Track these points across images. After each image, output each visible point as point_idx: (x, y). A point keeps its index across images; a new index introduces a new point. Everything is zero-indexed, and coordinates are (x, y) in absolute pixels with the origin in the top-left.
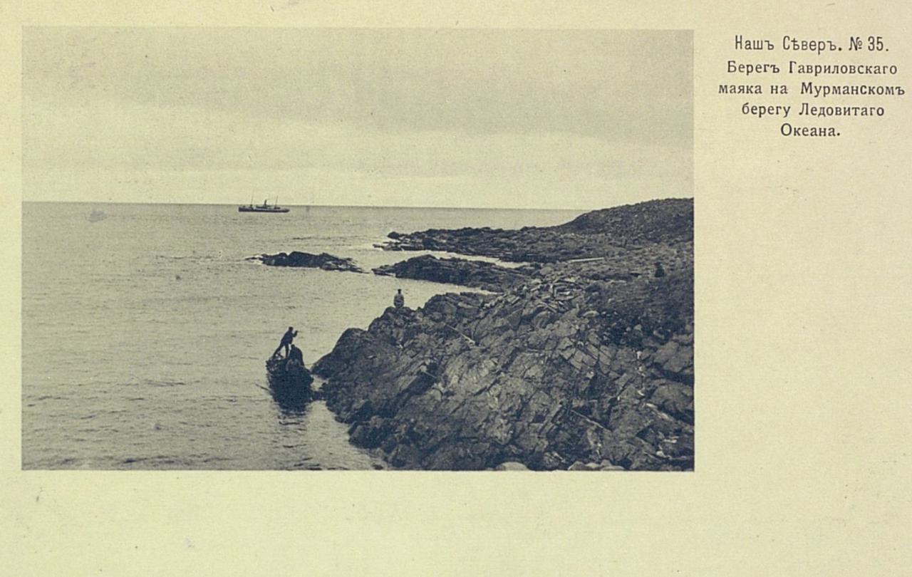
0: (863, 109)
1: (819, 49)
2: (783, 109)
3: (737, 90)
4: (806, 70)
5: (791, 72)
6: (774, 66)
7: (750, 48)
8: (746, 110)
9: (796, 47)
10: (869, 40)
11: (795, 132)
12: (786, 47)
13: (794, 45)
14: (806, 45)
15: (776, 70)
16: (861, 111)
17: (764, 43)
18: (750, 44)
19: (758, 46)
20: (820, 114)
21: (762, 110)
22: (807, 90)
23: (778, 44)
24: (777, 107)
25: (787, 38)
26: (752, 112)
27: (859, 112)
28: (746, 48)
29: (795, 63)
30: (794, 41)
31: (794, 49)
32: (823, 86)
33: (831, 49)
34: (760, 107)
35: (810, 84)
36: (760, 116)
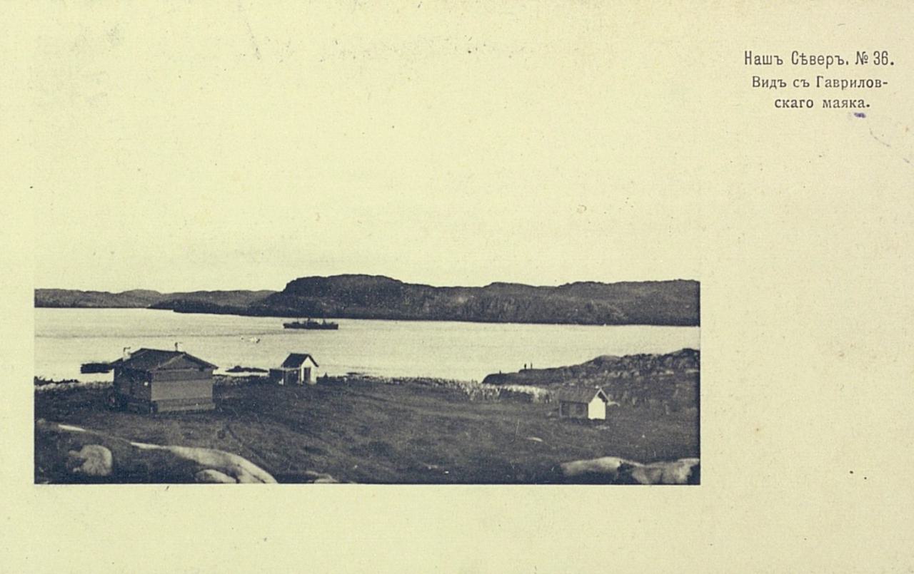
1: (828, 63)
4: (832, 84)
5: (818, 86)
6: (804, 81)
7: (760, 63)
9: (805, 62)
10: (875, 54)
12: (795, 61)
13: (803, 60)
14: (814, 60)
15: (783, 85)
17: (773, 58)
18: (759, 60)
23: (787, 59)
25: (795, 54)
28: (756, 64)
29: (822, 77)
30: (803, 56)
31: (803, 64)
33: (839, 64)
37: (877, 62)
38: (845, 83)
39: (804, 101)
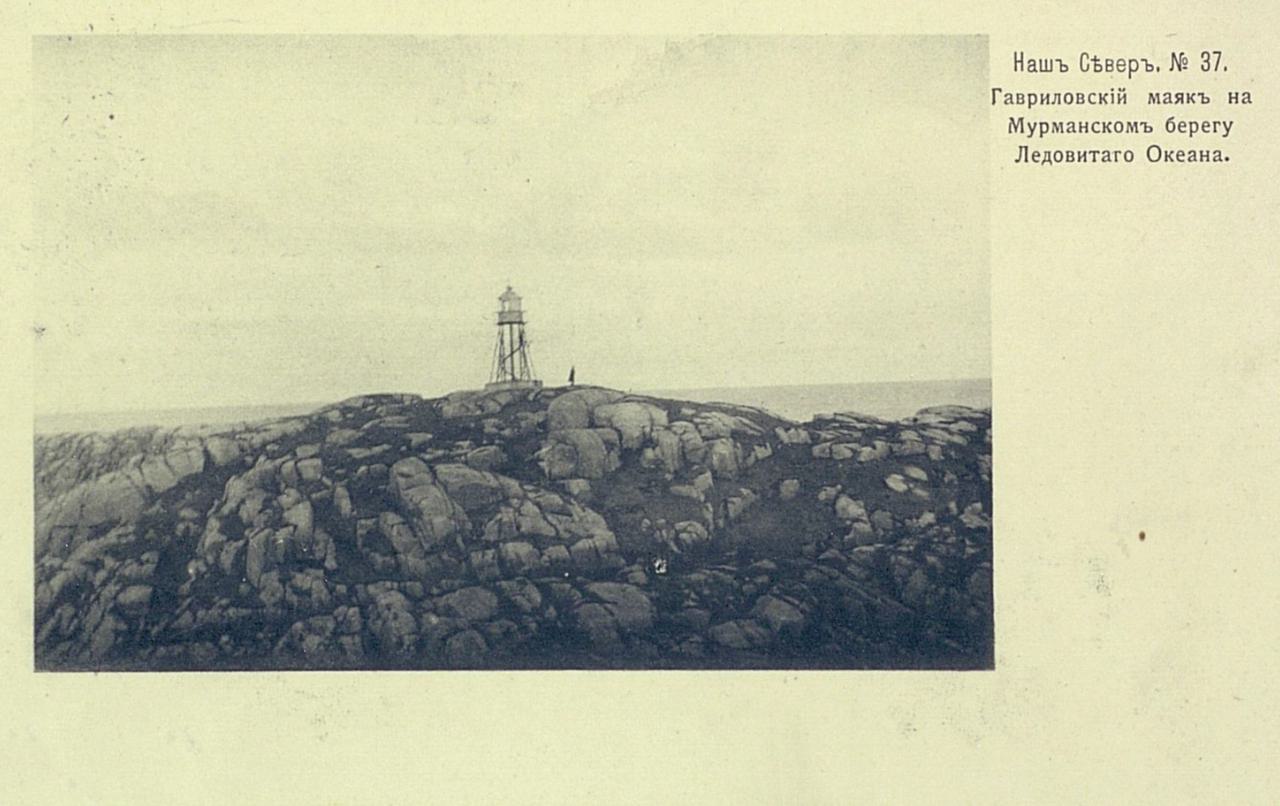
0: (1104, 153)
1: (1131, 70)
2: (1222, 125)
3: (1174, 99)
7: (1035, 70)
8: (1171, 127)
9: (1098, 68)
10: (1202, 56)
11: (1166, 156)
12: (1085, 68)
13: (1096, 65)
14: (1111, 65)
16: (1101, 156)
17: (1054, 62)
18: (1034, 65)
19: (1046, 66)
20: (1044, 161)
21: (1194, 126)
22: (1016, 128)
24: (1215, 123)
25: (1085, 56)
26: (1179, 130)
27: (1099, 157)
29: (1000, 90)
30: (1095, 60)
31: (1096, 71)
32: (1038, 122)
34: (1191, 123)
35: (1021, 119)
36: (1191, 136)
37: (1206, 68)
38: (1033, 98)
39: (1120, 152)
